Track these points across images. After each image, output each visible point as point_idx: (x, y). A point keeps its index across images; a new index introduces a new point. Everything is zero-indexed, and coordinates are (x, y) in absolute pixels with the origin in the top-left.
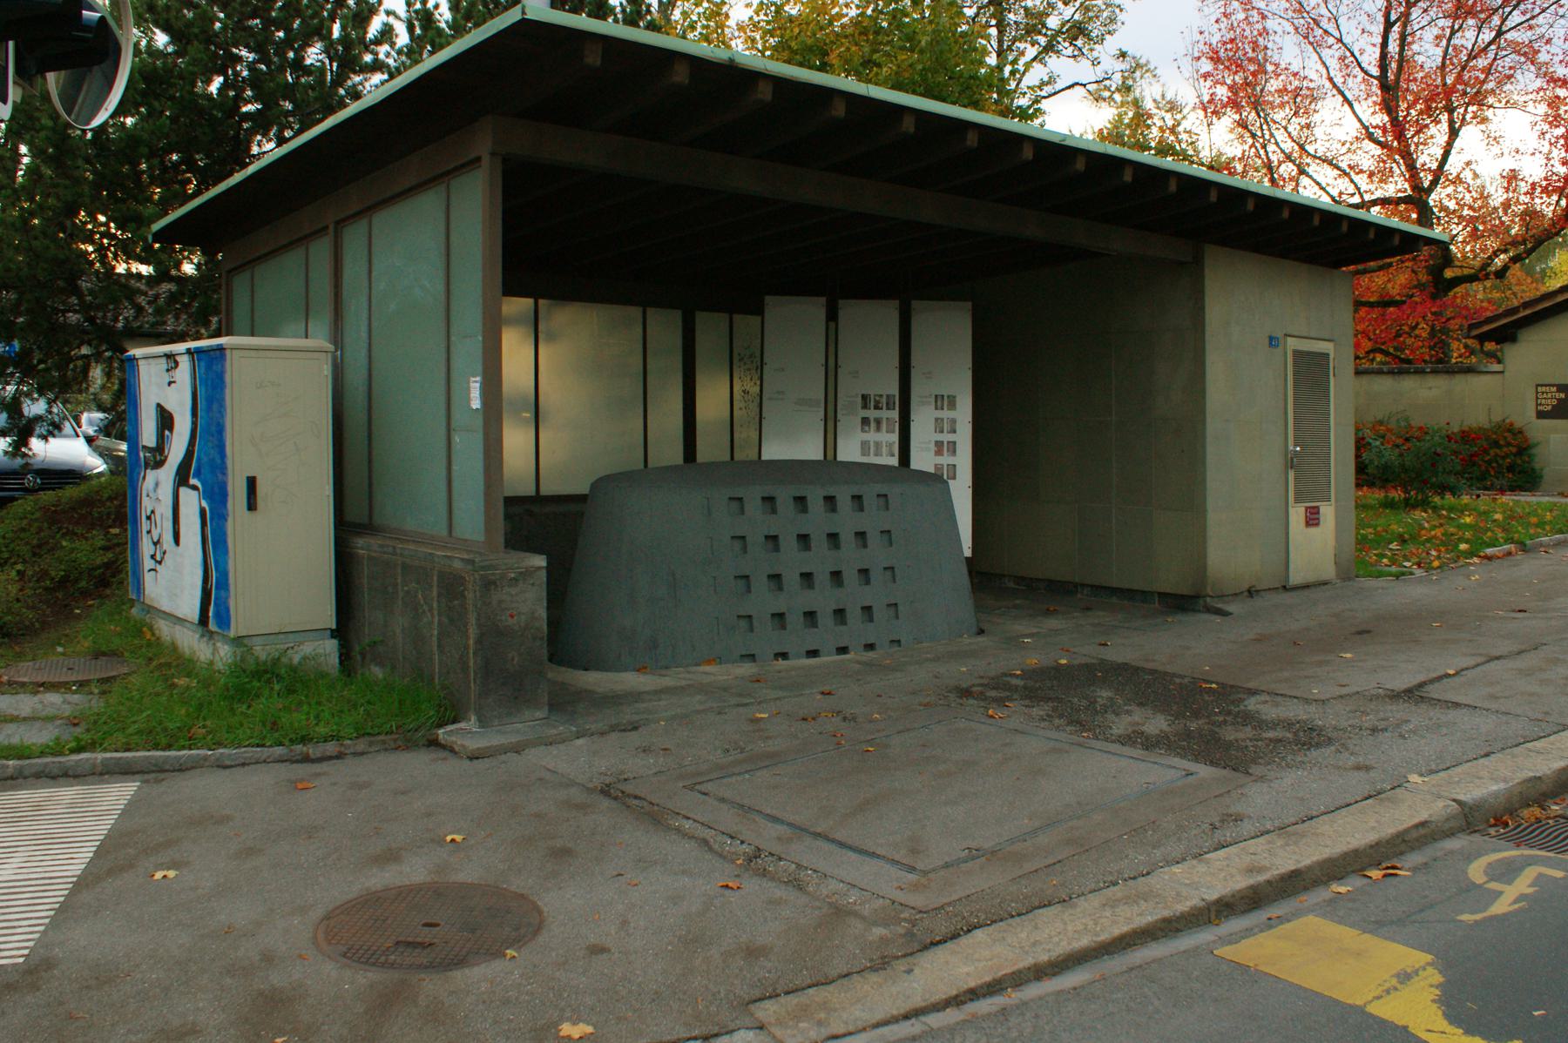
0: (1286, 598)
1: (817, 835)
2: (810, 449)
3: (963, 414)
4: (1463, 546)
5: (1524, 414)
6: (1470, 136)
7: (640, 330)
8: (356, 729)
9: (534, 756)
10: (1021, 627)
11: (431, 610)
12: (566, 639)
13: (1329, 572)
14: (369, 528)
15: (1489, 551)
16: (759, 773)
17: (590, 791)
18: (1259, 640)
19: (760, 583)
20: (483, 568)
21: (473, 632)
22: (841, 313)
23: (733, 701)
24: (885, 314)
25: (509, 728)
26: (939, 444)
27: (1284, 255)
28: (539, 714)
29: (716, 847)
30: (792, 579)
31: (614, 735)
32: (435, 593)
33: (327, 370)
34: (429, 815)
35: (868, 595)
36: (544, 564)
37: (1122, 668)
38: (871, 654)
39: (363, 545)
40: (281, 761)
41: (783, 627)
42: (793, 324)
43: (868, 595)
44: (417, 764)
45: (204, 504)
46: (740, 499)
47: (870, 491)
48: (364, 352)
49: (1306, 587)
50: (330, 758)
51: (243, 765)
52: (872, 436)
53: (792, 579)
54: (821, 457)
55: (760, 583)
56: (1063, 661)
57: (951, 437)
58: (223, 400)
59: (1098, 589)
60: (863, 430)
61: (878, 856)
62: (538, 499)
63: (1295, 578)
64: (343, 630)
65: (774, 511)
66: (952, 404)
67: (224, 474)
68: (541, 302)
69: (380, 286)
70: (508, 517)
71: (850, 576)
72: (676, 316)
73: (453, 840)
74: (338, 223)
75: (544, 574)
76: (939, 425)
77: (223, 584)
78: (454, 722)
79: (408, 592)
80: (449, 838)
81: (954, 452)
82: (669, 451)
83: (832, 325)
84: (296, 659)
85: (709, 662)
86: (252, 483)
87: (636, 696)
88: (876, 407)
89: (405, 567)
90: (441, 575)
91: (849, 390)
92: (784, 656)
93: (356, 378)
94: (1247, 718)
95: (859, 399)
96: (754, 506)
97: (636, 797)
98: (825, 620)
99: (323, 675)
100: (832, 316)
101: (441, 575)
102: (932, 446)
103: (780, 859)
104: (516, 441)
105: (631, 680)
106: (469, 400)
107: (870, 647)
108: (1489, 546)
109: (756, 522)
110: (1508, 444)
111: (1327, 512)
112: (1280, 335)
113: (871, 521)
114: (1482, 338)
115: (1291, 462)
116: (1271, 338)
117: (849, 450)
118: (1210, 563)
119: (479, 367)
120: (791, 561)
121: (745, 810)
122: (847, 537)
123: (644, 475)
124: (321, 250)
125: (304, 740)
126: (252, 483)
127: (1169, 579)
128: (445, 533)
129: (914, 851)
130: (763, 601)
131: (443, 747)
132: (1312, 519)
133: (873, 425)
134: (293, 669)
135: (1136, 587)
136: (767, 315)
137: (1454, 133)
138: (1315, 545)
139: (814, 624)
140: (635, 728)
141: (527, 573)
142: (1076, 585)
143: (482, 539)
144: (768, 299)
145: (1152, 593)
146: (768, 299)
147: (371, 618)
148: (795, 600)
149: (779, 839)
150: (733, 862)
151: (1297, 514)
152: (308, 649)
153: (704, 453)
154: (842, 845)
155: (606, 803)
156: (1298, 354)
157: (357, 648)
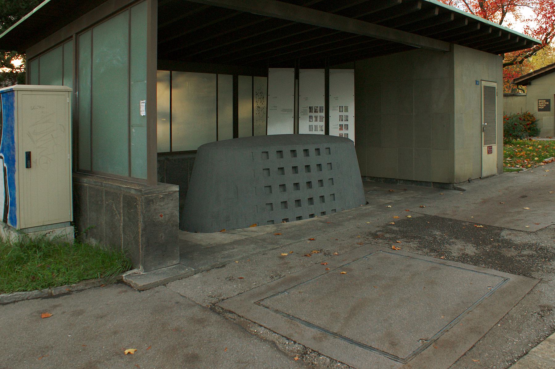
0: (481, 182)
1: (335, 335)
2: (287, 129)
4: (536, 159)
5: (534, 109)
6: (509, 16)
8: (79, 278)
9: (173, 286)
10: (383, 200)
11: (120, 213)
12: (187, 221)
13: (495, 171)
14: (90, 173)
15: (546, 160)
16: (292, 291)
17: (204, 308)
18: (484, 202)
19: (276, 189)
20: (146, 194)
21: (141, 225)
22: (300, 75)
23: (270, 247)
24: (318, 75)
25: (160, 271)
26: (341, 126)
27: (480, 49)
28: (175, 262)
29: (280, 347)
30: (290, 186)
31: (214, 271)
32: (122, 205)
33: (69, 100)
34: (115, 333)
35: (322, 191)
36: (178, 189)
37: (435, 219)
38: (324, 217)
39: (86, 182)
40: (36, 298)
41: (286, 207)
42: (280, 79)
43: (322, 191)
44: (111, 296)
45: (5, 165)
48: (89, 92)
49: (487, 177)
50: (64, 294)
51: (14, 302)
52: (314, 123)
53: (290, 186)
54: (293, 133)
55: (276, 189)
56: (410, 216)
57: (346, 123)
58: (13, 115)
59: (406, 181)
61: (374, 349)
62: (171, 153)
63: (484, 174)
64: (76, 222)
65: (282, 157)
66: (347, 110)
67: (14, 151)
68: (173, 72)
69: (96, 61)
70: (159, 161)
71: (315, 184)
72: (231, 77)
73: (129, 353)
74: (77, 34)
75: (178, 194)
77: (13, 204)
78: (131, 269)
79: (108, 205)
80: (127, 352)
82: (227, 132)
83: (297, 80)
84: (51, 238)
85: (253, 225)
86: (28, 155)
87: (221, 247)
88: (315, 112)
89: (107, 193)
90: (125, 197)
91: (304, 105)
92: (287, 220)
93: (85, 104)
94: (509, 244)
97: (230, 312)
98: (305, 203)
99: (66, 245)
100: (297, 77)
101: (125, 197)
102: (339, 127)
103: (319, 354)
104: (162, 129)
105: (218, 237)
106: (140, 111)
107: (323, 213)
108: (545, 158)
109: (274, 162)
110: (528, 120)
111: (495, 148)
112: (479, 80)
113: (324, 159)
114: (518, 84)
115: (483, 129)
116: (476, 81)
117: (304, 129)
118: (456, 170)
119: (145, 96)
120: (290, 178)
121: (292, 318)
122: (313, 167)
123: (217, 143)
124: (69, 46)
125: (50, 285)
126: (28, 155)
128: (127, 175)
129: (393, 344)
130: (277, 197)
131: (125, 284)
132: (490, 151)
133: (314, 119)
134: (49, 244)
136: (269, 76)
137: (504, 15)
138: (491, 161)
139: (300, 205)
140: (224, 266)
141: (170, 194)
142: (397, 180)
143: (146, 178)
144: (269, 69)
145: (430, 182)
146: (269, 69)
147: (89, 216)
148: (291, 195)
149: (314, 338)
150: (292, 358)
151: (485, 149)
152: (58, 232)
154: (352, 341)
155: (214, 317)
156: (485, 87)
157: (84, 230)
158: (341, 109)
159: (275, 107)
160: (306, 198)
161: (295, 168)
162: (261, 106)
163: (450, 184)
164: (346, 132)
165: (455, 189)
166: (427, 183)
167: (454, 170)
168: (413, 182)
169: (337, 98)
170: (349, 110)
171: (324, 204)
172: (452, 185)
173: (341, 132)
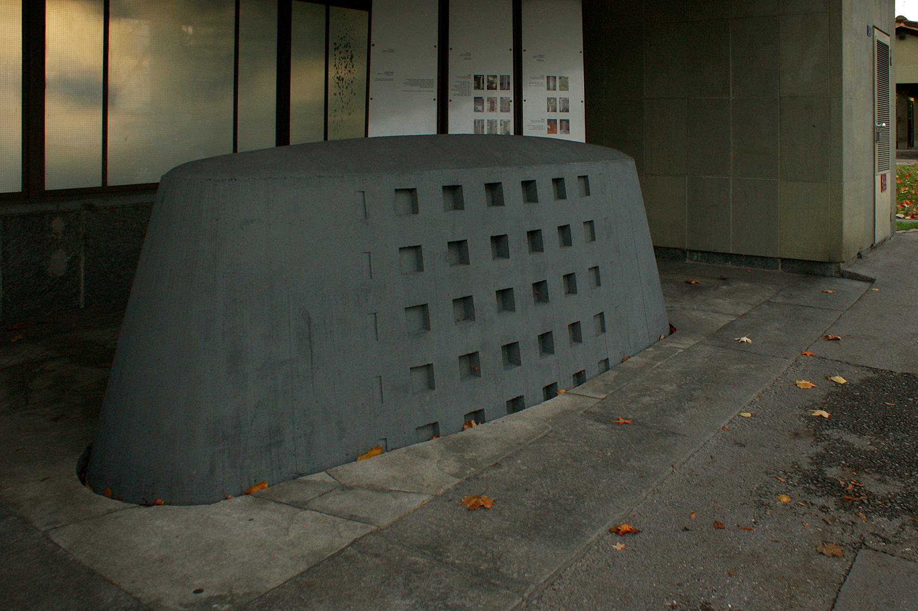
3: (576, 94)
7: (233, 13)
19: (444, 314)
26: (552, 123)
46: (412, 191)
47: (571, 172)
53: (485, 301)
55: (444, 314)
59: (710, 255)
60: (476, 110)
62: (105, 190)
66: (565, 86)
76: (551, 105)
81: (567, 130)
82: (259, 132)
88: (490, 88)
95: (472, 80)
96: (432, 199)
98: (529, 352)
109: (436, 224)
123: (233, 163)
127: (798, 244)
130: (448, 340)
133: (487, 105)
135: (743, 253)
142: (684, 252)
148: (491, 331)
153: (296, 136)
158: (551, 84)
159: (387, 73)
160: (534, 338)
161: (499, 242)
162: (347, 77)
163: (830, 263)
165: (843, 275)
166: (766, 261)
167: (842, 233)
168: (749, 260)
169: (540, 58)
170: (570, 85)
171: (580, 347)
172: (833, 267)
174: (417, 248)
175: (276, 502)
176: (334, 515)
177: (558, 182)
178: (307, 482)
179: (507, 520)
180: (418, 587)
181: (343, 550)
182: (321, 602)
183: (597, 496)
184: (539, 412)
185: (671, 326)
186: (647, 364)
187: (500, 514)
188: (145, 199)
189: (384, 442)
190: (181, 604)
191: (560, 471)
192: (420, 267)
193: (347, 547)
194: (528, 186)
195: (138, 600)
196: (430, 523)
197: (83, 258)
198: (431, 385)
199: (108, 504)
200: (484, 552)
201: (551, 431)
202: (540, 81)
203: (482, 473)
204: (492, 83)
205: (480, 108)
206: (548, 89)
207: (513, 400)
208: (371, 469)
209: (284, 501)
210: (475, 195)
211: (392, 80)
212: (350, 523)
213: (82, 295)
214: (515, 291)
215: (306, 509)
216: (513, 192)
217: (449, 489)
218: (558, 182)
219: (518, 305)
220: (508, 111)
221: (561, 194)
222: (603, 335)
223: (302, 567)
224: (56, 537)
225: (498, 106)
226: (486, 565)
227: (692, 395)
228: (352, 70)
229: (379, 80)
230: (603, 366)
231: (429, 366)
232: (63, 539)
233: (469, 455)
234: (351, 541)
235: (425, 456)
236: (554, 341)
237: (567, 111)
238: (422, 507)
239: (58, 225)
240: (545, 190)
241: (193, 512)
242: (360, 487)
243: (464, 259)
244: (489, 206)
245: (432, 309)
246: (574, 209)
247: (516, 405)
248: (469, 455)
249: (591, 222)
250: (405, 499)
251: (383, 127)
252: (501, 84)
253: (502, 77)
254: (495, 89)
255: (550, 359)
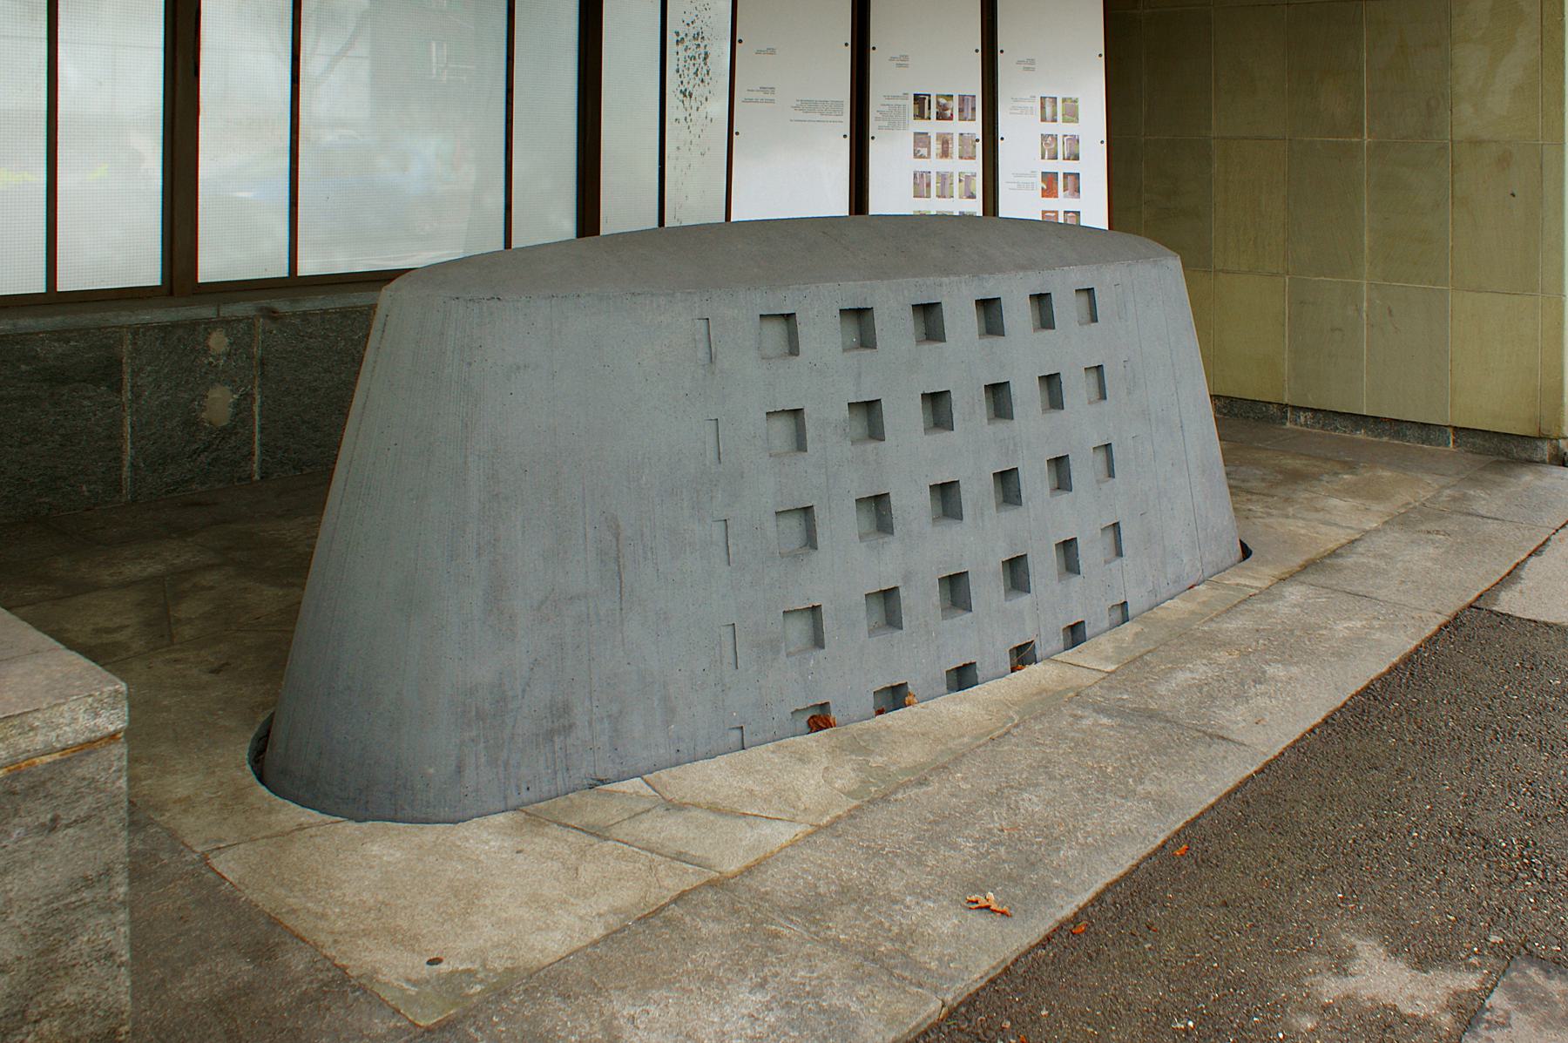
2: (795, 179)
19: (841, 523)
26: (1049, 178)
46: (789, 317)
47: (1063, 284)
52: (934, 165)
53: (911, 503)
55: (841, 523)
66: (1072, 115)
75: (120, 750)
76: (1049, 147)
82: (549, 215)
88: (940, 117)
96: (822, 332)
98: (987, 588)
102: (1040, 185)
109: (828, 375)
127: (1487, 402)
130: (847, 567)
142: (1283, 407)
148: (920, 552)
153: (612, 219)
161: (937, 404)
164: (1072, 204)
166: (1426, 430)
168: (1396, 426)
169: (1029, 65)
171: (1076, 580)
173: (1050, 204)
174: (797, 413)
175: (559, 824)
176: (652, 852)
177: (1041, 300)
178: (611, 793)
179: (929, 874)
180: (776, 975)
181: (662, 908)
182: (623, 989)
183: (1081, 840)
184: (999, 690)
185: (1244, 546)
186: (1193, 613)
187: (920, 863)
188: (358, 299)
189: (738, 733)
190: (408, 980)
191: (1025, 795)
192: (801, 445)
193: (667, 905)
194: (988, 308)
195: (343, 969)
196: (805, 871)
197: (258, 397)
198: (818, 642)
199: (291, 814)
200: (887, 925)
201: (1017, 726)
202: (1029, 105)
203: (895, 792)
204: (945, 108)
205: (924, 151)
206: (1044, 119)
207: (958, 669)
208: (714, 777)
209: (572, 823)
210: (895, 324)
211: (772, 101)
212: (677, 864)
213: (256, 458)
214: (963, 487)
215: (607, 839)
216: (961, 319)
217: (839, 817)
218: (1041, 300)
219: (967, 510)
220: (973, 158)
221: (1046, 320)
222: (1118, 561)
223: (598, 932)
224: (221, 863)
225: (955, 148)
226: (889, 945)
227: (1264, 672)
228: (707, 79)
229: (751, 101)
230: (1117, 615)
231: (815, 609)
232: (228, 865)
233: (877, 761)
234: (675, 894)
235: (803, 759)
236: (1031, 571)
237: (1077, 158)
238: (793, 844)
239: (218, 341)
240: (1018, 314)
241: (430, 834)
242: (697, 806)
243: (875, 432)
244: (919, 342)
245: (820, 515)
246: (1069, 348)
247: (962, 677)
248: (877, 761)
249: (1099, 368)
250: (766, 829)
251: (755, 202)
252: (961, 111)
253: (962, 98)
254: (951, 118)
255: (1024, 600)
